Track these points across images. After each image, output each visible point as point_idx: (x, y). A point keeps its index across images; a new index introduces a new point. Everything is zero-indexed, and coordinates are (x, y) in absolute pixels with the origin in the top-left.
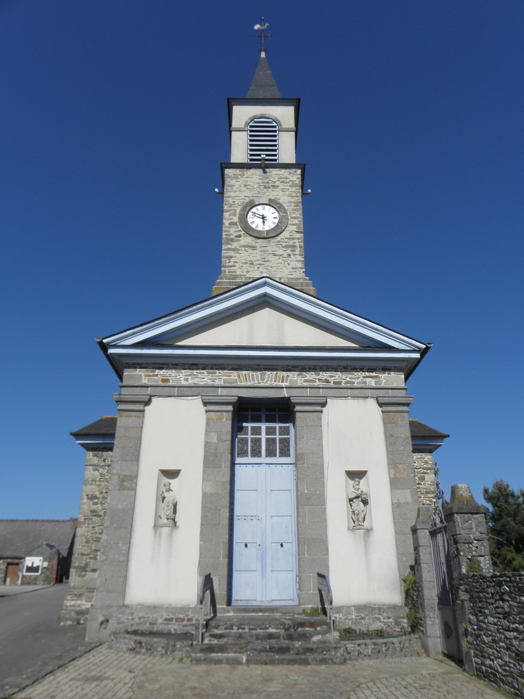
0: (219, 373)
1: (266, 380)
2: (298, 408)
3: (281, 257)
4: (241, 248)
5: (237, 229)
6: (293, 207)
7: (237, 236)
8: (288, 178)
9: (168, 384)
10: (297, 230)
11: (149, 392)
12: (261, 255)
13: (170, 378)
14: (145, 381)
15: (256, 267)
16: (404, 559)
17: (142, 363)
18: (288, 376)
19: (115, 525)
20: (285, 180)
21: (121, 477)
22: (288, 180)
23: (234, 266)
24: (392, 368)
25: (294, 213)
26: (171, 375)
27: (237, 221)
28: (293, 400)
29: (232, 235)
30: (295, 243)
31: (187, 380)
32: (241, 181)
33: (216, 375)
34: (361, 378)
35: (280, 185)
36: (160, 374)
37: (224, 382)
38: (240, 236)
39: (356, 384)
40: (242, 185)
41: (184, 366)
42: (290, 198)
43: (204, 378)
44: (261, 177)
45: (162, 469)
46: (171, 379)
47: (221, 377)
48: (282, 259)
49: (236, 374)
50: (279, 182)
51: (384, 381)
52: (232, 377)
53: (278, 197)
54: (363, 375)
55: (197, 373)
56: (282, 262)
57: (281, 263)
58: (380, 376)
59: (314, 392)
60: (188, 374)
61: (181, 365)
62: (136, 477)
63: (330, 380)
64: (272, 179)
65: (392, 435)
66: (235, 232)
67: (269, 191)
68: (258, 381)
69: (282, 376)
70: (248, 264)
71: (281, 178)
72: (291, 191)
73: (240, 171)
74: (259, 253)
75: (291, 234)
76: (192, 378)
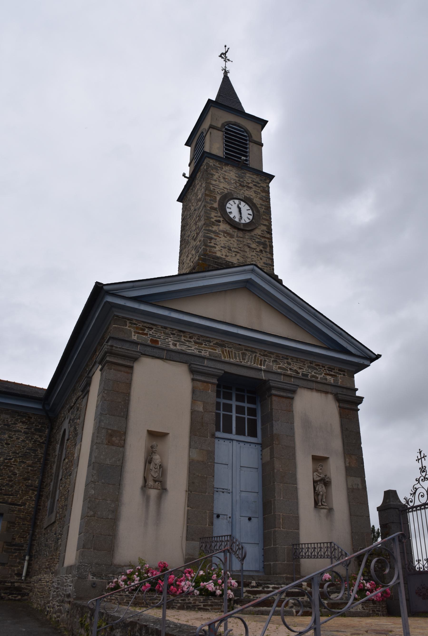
0: (205, 345)
1: (246, 360)
3: (255, 251)
4: (220, 233)
5: (216, 215)
6: (264, 209)
7: (216, 221)
8: (260, 184)
9: (157, 346)
10: (266, 230)
11: (138, 349)
12: (238, 244)
13: (159, 340)
14: (135, 337)
15: (234, 254)
16: (357, 537)
17: (132, 319)
18: (265, 361)
19: (103, 481)
20: (257, 184)
21: (110, 431)
22: (259, 185)
23: (215, 247)
24: (346, 371)
25: (264, 215)
26: (161, 337)
27: (217, 207)
29: (213, 218)
30: (266, 241)
31: (175, 345)
32: (220, 173)
33: (202, 346)
34: (323, 375)
35: (253, 188)
36: (150, 334)
37: (210, 355)
38: (219, 221)
39: (319, 379)
40: (221, 177)
41: (173, 331)
42: (261, 201)
43: (191, 347)
44: (237, 175)
45: (150, 429)
46: (160, 341)
47: (207, 349)
48: (255, 252)
49: (220, 348)
50: (252, 184)
51: (340, 380)
52: (217, 351)
53: (252, 197)
54: (325, 372)
55: (185, 340)
56: (256, 255)
57: (255, 256)
58: (338, 375)
59: (287, 380)
60: (176, 339)
61: (169, 329)
62: (125, 433)
63: (299, 371)
64: (246, 180)
65: (347, 428)
66: (215, 216)
67: (244, 189)
68: (240, 360)
69: (260, 360)
70: (227, 249)
71: (253, 182)
72: (262, 195)
73: (219, 164)
74: (236, 241)
75: (262, 232)
76: (180, 344)
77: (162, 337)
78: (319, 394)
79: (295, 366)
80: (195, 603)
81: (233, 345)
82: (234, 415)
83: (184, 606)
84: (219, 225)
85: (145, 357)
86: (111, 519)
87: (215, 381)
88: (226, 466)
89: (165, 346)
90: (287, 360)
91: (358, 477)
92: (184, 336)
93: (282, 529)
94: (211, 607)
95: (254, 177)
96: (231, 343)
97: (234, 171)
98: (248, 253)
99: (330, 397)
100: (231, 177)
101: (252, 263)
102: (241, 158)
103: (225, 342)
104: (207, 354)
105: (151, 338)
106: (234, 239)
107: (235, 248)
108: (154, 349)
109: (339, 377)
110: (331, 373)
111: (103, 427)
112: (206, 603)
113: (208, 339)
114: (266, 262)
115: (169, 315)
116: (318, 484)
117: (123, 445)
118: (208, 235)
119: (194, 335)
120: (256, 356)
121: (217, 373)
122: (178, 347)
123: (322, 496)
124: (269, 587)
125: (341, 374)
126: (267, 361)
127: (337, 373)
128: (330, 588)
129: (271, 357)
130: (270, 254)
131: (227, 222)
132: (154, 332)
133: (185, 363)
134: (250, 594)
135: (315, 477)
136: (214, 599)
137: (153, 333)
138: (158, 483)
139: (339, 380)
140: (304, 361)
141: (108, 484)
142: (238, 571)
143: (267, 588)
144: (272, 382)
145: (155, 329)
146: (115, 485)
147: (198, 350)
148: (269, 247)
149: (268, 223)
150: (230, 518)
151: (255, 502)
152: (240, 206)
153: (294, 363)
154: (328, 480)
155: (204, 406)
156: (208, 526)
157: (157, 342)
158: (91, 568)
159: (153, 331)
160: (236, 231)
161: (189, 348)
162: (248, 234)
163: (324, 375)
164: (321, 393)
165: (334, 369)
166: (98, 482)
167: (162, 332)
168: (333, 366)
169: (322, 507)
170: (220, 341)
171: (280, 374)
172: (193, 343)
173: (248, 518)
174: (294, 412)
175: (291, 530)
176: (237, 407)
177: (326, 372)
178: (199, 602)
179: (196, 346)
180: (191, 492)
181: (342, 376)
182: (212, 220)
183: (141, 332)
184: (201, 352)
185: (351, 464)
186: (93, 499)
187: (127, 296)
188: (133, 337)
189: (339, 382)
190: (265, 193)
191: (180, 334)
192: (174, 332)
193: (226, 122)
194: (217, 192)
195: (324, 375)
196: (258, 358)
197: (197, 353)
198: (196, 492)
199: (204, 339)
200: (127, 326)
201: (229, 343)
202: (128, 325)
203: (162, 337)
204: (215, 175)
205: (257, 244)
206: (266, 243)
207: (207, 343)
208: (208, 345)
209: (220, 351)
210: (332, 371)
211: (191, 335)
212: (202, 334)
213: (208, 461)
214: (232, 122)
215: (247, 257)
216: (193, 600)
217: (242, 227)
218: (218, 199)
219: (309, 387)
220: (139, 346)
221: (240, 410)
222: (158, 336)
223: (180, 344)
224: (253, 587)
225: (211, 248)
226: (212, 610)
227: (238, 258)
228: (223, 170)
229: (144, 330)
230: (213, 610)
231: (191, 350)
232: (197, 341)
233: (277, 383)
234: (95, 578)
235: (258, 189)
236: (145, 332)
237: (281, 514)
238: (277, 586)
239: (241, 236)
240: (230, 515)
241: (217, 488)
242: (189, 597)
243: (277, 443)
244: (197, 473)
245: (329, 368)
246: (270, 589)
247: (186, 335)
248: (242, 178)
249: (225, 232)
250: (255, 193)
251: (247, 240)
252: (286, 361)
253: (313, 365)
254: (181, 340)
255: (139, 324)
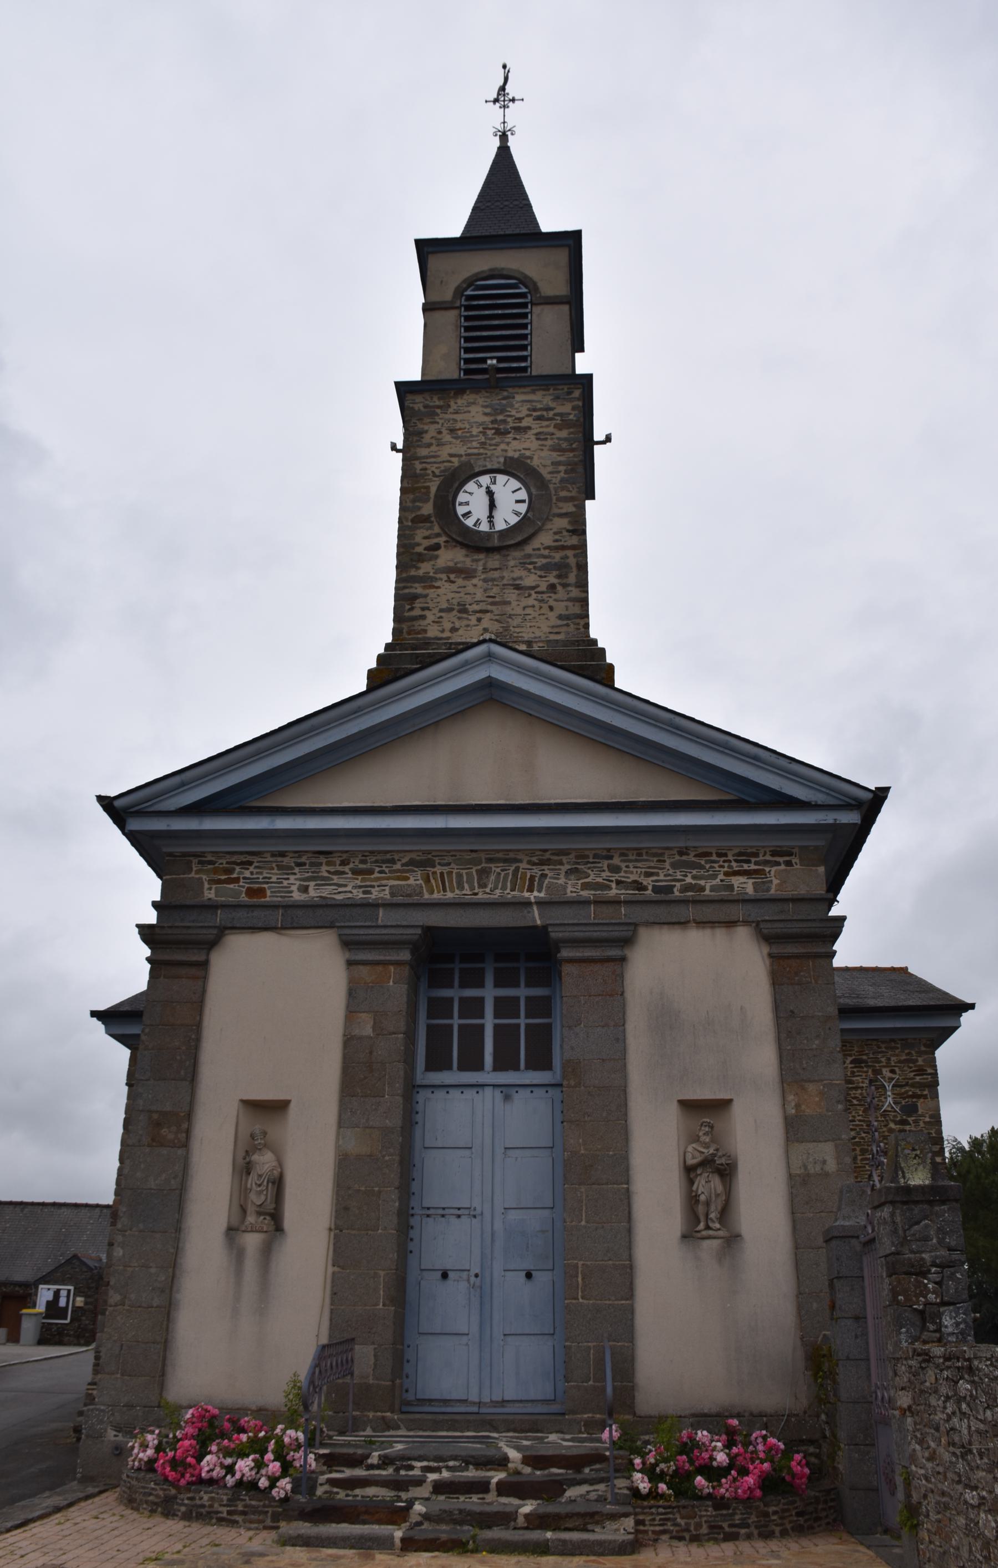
0: (380, 872)
1: (490, 886)
2: (565, 953)
3: (533, 592)
5: (427, 533)
6: (562, 474)
10: (570, 528)
12: (485, 590)
13: (266, 886)
14: (210, 894)
15: (473, 619)
16: (815, 1305)
17: (204, 853)
19: (141, 1226)
20: (545, 413)
21: (155, 1116)
22: (551, 414)
26: (270, 878)
28: (555, 934)
29: (419, 545)
30: (567, 557)
31: (305, 889)
33: (372, 876)
34: (721, 877)
35: (533, 426)
36: (244, 878)
37: (392, 894)
38: (437, 547)
39: (707, 892)
41: (300, 857)
42: (554, 454)
43: (345, 886)
44: (488, 410)
45: (245, 1098)
46: (269, 888)
47: (384, 882)
48: (534, 596)
49: (419, 872)
50: (530, 419)
51: (776, 882)
54: (726, 869)
55: (328, 872)
56: (536, 603)
57: (533, 606)
58: (767, 869)
60: (307, 875)
61: (292, 855)
62: (189, 1116)
63: (645, 883)
64: (513, 413)
65: (792, 1012)
67: (507, 440)
68: (472, 888)
69: (528, 877)
70: (455, 613)
71: (535, 410)
75: (557, 537)
76: (316, 885)
77: (274, 879)
78: (708, 932)
79: (632, 873)
80: (211, 1506)
81: (455, 856)
82: (489, 1022)
83: (191, 1512)
84: (437, 557)
85: (235, 933)
86: (157, 1307)
87: (405, 955)
88: (467, 1152)
89: (281, 897)
90: (610, 862)
91: (826, 1141)
92: (328, 864)
93: (581, 1300)
94: (243, 1517)
95: (538, 396)
96: (449, 851)
97: (481, 401)
98: (514, 604)
99: (743, 934)
100: (472, 420)
101: (481, 638)
102: (498, 362)
103: (433, 854)
104: (386, 894)
105: (247, 885)
106: (475, 581)
107: (478, 602)
108: (253, 911)
109: (772, 873)
110: (746, 867)
111: (141, 1108)
112: (233, 1508)
113: (388, 856)
114: (567, 613)
115: (271, 827)
116: (697, 1176)
117: (185, 1142)
118: (407, 591)
119: (353, 854)
120: (517, 869)
121: (405, 937)
122: (312, 893)
123: (708, 1204)
124: (411, 1468)
125: (778, 864)
126: (550, 874)
127: (766, 863)
128: (593, 1467)
129: (561, 863)
130: (577, 587)
131: (457, 542)
132: (255, 871)
133: (331, 926)
134: (337, 1487)
135: (689, 1156)
136: (250, 1500)
137: (252, 873)
138: (265, 1219)
139: (771, 882)
140: (660, 851)
141: (153, 1232)
142: (497, 1402)
143: (407, 1470)
144: (556, 929)
145: (258, 862)
146: (166, 1232)
147: (361, 890)
148: (574, 569)
149: (575, 506)
150: (476, 1276)
151: (543, 1232)
152: (493, 488)
153: (631, 865)
154: (723, 1161)
155: (375, 1023)
156: (381, 1306)
157: (261, 892)
158: (113, 1414)
159: (251, 869)
160: (482, 556)
161: (341, 889)
162: (517, 554)
163: (724, 878)
164: (712, 927)
165: (756, 855)
166: (131, 1230)
167: (274, 865)
168: (751, 847)
169: (705, 1233)
170: (420, 854)
171: (585, 903)
172: (350, 875)
173: (525, 1272)
174: (628, 995)
175: (607, 1302)
176: (497, 1000)
177: (730, 867)
178: (221, 1505)
179: (357, 879)
180: (341, 1231)
181: (783, 867)
182: (419, 549)
183: (223, 877)
184: (369, 893)
185: (803, 1107)
186: (121, 1268)
187: (173, 809)
188: (206, 894)
189: (773, 887)
190: (568, 428)
191: (317, 860)
192: (303, 859)
193: (464, 281)
194: (433, 472)
195: (724, 878)
196: (524, 874)
197: (361, 896)
198: (354, 1229)
199: (379, 857)
200: (193, 872)
201: (445, 854)
202: (194, 869)
203: (274, 879)
204: (426, 432)
205: (539, 573)
206: (567, 561)
207: (384, 866)
208: (387, 870)
209: (418, 880)
210: (748, 862)
211: (345, 856)
212: (370, 848)
213: (384, 1153)
214: (483, 272)
215: (510, 616)
216: (208, 1501)
217: (496, 542)
218: (433, 490)
219: (674, 920)
220: (219, 912)
221: (505, 1007)
222: (264, 878)
223: (316, 885)
224: (371, 1467)
225: (414, 623)
226: (245, 1523)
227: (485, 626)
228: (451, 410)
229: (231, 871)
230: (248, 1525)
231: (346, 892)
232: (361, 866)
233: (570, 929)
234: (120, 1435)
235: (547, 426)
236: (235, 876)
237: (580, 1263)
238: (436, 1464)
239: (496, 564)
240: (477, 1271)
241: (444, 1209)
242: (202, 1493)
243: (572, 1083)
244: (356, 1185)
245: (740, 854)
246: (416, 1472)
247: (334, 859)
248: (502, 411)
249: (449, 570)
250: (538, 439)
251: (512, 571)
252: (606, 863)
253: (691, 858)
254: (320, 874)
255: (220, 861)
